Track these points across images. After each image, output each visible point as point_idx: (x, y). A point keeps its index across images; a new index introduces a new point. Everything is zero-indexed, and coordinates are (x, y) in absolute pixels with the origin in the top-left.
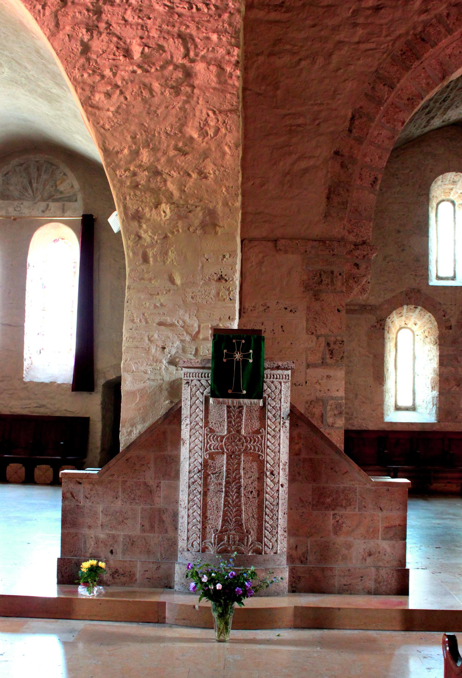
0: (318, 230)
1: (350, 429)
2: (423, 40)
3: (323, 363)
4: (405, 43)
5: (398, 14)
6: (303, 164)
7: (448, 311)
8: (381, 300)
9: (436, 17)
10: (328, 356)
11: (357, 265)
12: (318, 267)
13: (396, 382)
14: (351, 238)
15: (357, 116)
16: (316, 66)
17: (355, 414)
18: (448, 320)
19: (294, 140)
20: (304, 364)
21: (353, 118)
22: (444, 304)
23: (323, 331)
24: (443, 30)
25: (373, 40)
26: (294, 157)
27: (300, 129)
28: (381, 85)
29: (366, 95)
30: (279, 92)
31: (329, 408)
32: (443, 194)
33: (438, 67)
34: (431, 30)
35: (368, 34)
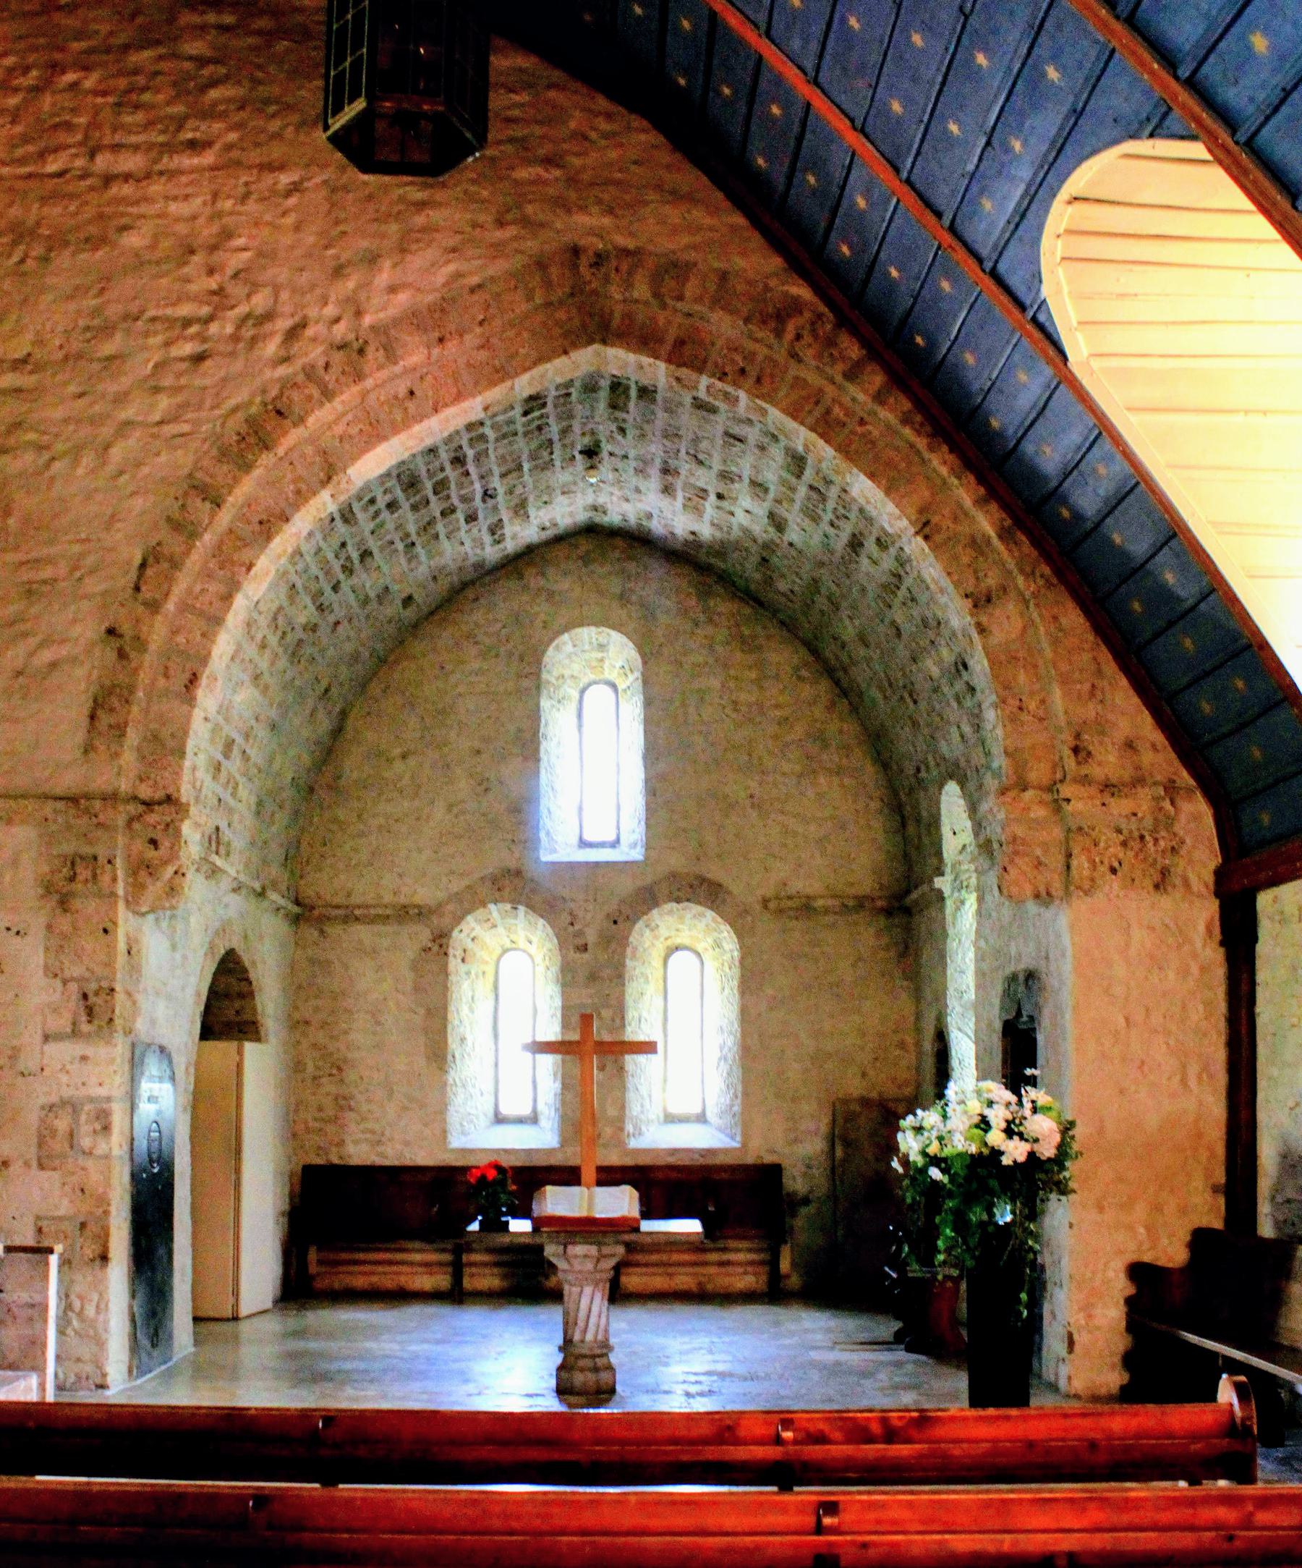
0: (69, 781)
2: (279, 413)
3: (75, 1033)
5: (238, 365)
7: (581, 914)
8: (441, 895)
10: (84, 1018)
11: (154, 843)
12: (68, 848)
15: (151, 560)
17: (387, 1133)
18: (580, 934)
19: (33, 611)
21: (143, 565)
23: (77, 971)
24: (315, 392)
26: (33, 641)
27: (45, 588)
28: (198, 501)
29: (169, 519)
31: (83, 1118)
34: (296, 396)
35: (179, 406)
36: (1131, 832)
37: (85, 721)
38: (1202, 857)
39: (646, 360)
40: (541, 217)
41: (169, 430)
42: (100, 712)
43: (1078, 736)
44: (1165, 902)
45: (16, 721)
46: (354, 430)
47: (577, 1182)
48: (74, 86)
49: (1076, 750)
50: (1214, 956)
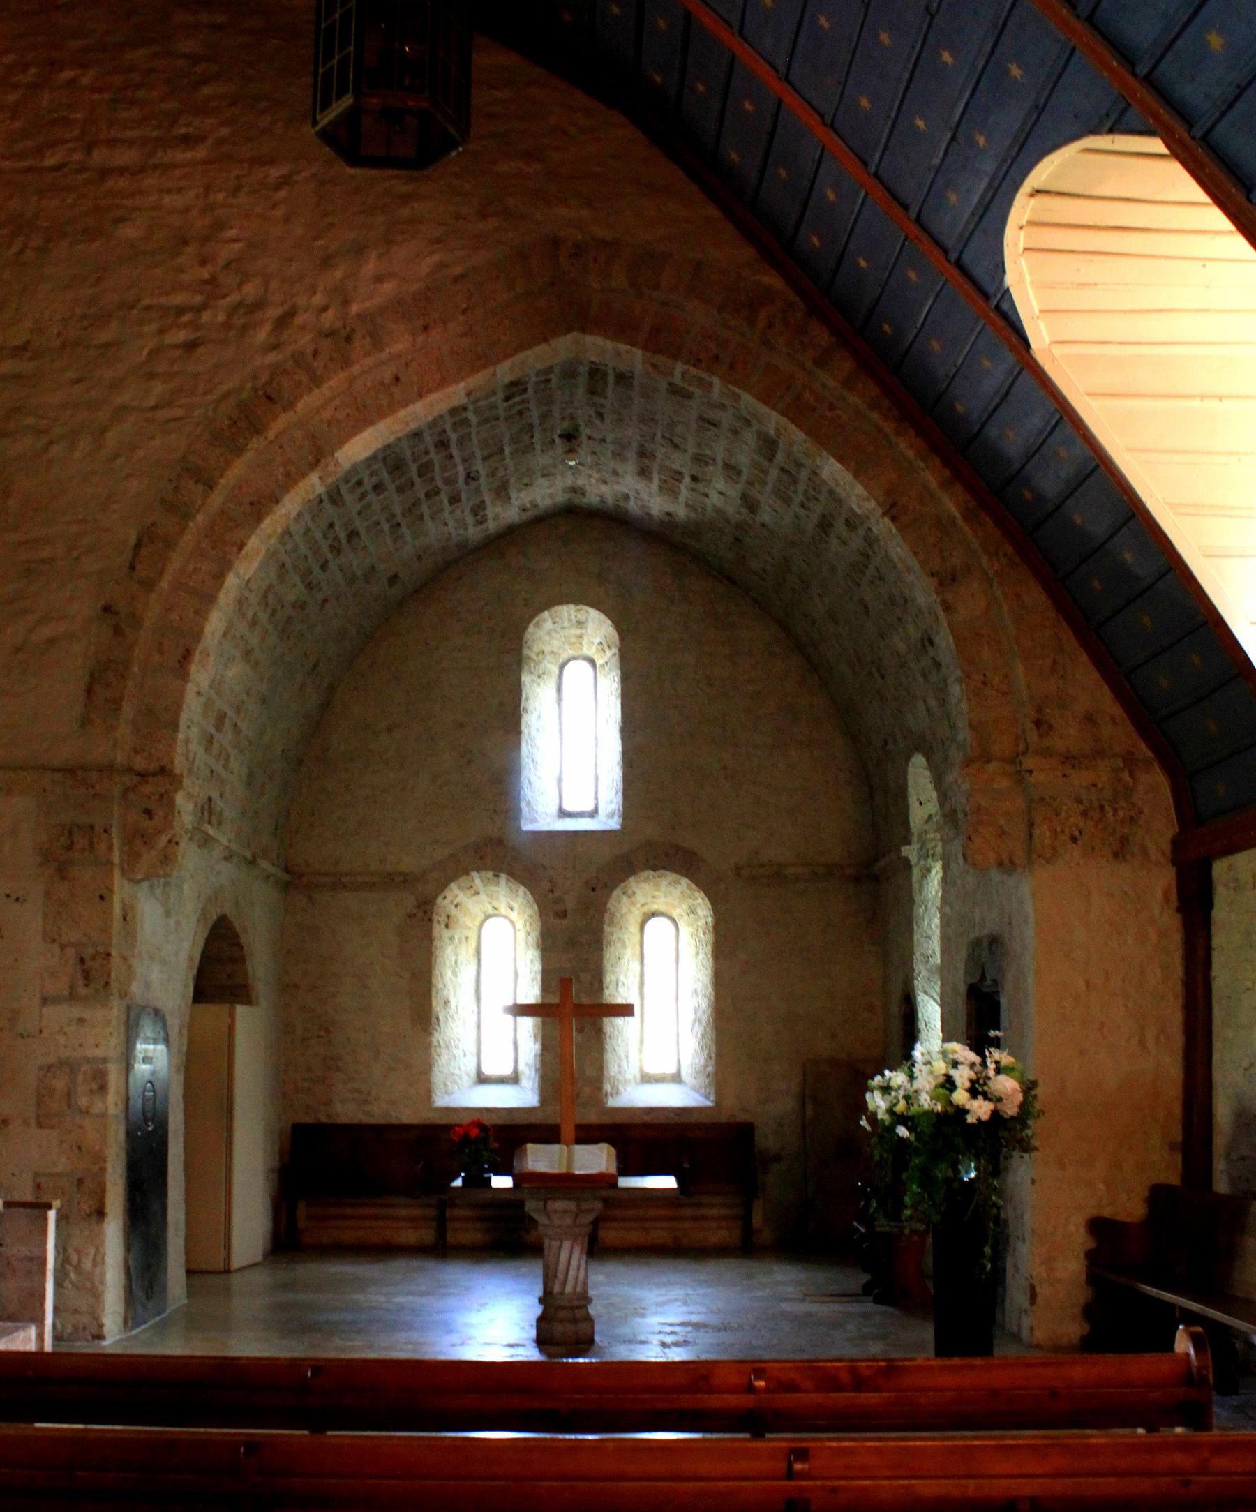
2: (269, 398)
3: (73, 997)
4: (238, 405)
9: (293, 356)
10: (81, 982)
11: (148, 813)
13: (479, 1027)
14: (140, 763)
16: (77, 455)
18: (559, 900)
21: (138, 545)
22: (552, 868)
24: (304, 379)
25: (183, 401)
29: (163, 501)
30: (11, 503)
31: (80, 1078)
32: (567, 647)
33: (306, 443)
36: (1091, 802)
41: (162, 414)
43: (1039, 710)
46: (341, 415)
48: (71, 83)
49: (1038, 723)
50: (1170, 921)
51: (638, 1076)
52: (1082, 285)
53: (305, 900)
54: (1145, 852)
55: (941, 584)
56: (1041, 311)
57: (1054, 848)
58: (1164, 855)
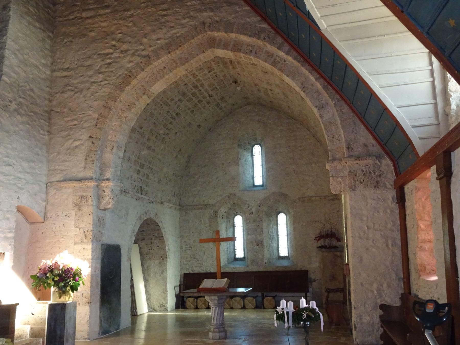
1: (196, 272)
3: (82, 242)
6: (77, 143)
7: (251, 204)
10: (84, 238)
12: (80, 194)
17: (204, 264)
20: (73, 243)
23: (82, 225)
36: (366, 171)
37: (84, 160)
38: (391, 176)
39: (226, 51)
40: (196, 15)
41: (102, 83)
42: (88, 158)
43: (349, 144)
44: (378, 191)
45: (69, 161)
46: (151, 79)
47: (216, 278)
49: (348, 148)
50: (395, 206)
51: (277, 257)
52: (333, 5)
53: (185, 213)
54: (385, 185)
55: (319, 109)
56: (321, 17)
57: (355, 186)
58: (391, 185)
